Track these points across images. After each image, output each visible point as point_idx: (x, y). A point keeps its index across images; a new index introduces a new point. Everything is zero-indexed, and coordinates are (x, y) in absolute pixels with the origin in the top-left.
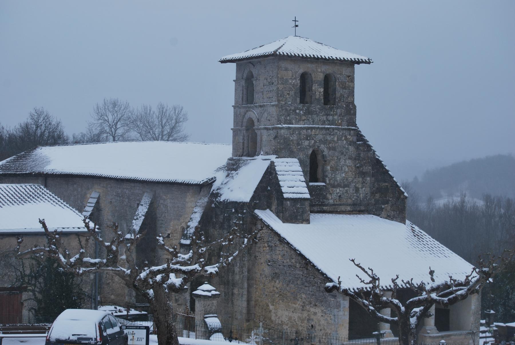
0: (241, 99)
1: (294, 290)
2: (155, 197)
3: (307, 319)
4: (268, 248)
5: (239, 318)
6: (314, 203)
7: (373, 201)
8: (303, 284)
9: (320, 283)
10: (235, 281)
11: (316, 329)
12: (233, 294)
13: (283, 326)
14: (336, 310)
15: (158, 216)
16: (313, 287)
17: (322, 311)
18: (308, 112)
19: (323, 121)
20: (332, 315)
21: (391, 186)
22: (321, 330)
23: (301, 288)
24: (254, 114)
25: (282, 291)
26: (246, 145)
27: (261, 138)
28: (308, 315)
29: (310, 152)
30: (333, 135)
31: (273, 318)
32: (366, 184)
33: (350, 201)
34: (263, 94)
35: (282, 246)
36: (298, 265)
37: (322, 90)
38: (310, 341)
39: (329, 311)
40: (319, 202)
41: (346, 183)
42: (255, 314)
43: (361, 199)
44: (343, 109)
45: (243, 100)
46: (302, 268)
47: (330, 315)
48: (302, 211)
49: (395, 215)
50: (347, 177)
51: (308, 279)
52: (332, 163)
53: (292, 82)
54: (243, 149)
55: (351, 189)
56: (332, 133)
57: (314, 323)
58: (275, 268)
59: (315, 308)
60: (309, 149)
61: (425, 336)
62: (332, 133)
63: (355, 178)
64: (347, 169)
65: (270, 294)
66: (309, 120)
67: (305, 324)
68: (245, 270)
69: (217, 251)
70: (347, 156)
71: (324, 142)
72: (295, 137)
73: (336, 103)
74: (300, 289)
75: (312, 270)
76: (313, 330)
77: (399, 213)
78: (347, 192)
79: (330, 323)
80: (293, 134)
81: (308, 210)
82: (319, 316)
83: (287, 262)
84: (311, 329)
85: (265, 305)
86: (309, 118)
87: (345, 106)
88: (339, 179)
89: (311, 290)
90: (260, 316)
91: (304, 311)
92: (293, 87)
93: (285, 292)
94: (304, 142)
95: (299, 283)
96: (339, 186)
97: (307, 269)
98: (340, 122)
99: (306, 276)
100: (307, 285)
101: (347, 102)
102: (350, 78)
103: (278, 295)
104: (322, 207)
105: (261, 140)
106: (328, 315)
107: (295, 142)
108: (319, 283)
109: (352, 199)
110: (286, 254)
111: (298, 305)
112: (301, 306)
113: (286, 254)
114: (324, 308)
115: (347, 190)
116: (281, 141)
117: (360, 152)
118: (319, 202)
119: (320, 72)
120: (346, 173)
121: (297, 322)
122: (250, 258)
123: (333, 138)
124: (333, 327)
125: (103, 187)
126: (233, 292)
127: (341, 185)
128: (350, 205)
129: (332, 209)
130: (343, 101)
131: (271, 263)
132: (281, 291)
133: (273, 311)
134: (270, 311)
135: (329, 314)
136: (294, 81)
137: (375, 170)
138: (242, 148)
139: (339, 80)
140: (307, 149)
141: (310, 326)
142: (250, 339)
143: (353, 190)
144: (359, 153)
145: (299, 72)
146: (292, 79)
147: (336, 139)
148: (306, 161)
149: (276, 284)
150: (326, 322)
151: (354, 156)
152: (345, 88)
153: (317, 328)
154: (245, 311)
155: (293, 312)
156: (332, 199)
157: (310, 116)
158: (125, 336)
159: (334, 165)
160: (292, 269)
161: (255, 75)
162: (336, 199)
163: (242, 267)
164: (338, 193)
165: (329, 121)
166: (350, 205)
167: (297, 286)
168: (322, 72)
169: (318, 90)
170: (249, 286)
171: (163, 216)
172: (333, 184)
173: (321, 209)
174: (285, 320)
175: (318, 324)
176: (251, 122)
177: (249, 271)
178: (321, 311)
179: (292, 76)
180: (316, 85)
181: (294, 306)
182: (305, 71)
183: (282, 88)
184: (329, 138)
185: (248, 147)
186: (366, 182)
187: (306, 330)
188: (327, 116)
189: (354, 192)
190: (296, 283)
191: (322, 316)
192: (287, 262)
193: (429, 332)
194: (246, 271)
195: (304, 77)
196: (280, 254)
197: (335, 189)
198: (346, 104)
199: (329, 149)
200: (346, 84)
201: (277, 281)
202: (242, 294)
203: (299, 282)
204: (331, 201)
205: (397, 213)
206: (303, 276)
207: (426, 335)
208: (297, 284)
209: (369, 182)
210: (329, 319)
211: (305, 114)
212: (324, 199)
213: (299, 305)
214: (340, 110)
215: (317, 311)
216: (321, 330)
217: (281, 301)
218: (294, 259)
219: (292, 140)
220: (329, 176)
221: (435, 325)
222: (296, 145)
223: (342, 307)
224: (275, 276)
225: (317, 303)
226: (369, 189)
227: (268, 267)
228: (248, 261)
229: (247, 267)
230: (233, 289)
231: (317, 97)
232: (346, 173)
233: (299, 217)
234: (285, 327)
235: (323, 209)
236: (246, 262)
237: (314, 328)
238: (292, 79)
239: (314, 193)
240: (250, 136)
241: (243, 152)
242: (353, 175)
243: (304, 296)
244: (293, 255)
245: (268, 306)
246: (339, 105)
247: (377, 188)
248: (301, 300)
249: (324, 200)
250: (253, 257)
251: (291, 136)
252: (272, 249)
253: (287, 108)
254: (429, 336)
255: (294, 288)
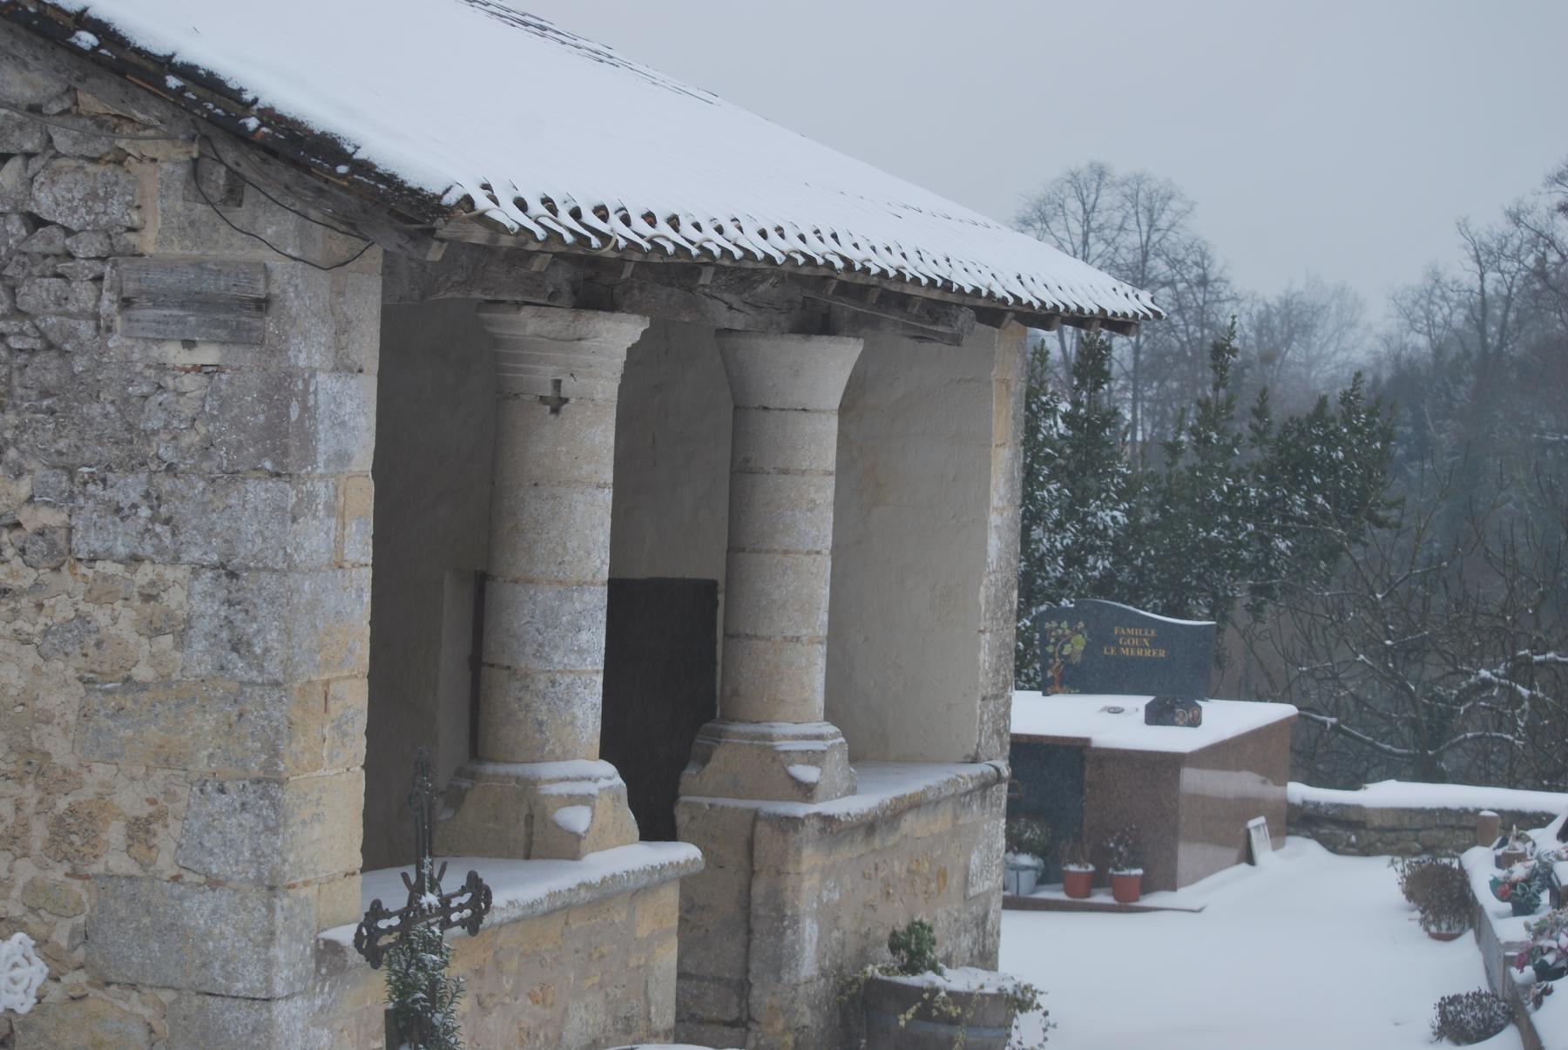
14: (258, 492)
47: (145, 573)
61: (794, 822)
79: (143, 673)
158: (1502, 817)
193: (808, 773)
207: (801, 810)
223: (321, 459)
254: (818, 815)
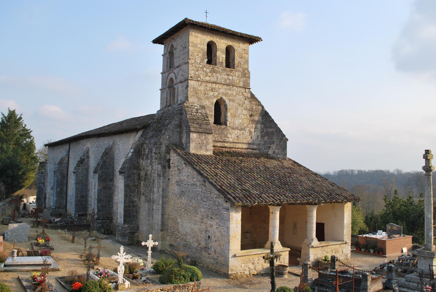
0: (166, 67)
1: (195, 205)
2: (114, 144)
3: (204, 230)
4: (177, 171)
5: (156, 228)
6: (217, 140)
7: (263, 142)
8: (202, 199)
9: (216, 198)
10: (154, 199)
11: (212, 240)
12: (153, 209)
13: (187, 236)
15: (115, 156)
16: (210, 202)
17: (217, 223)
18: (213, 71)
19: (225, 79)
20: (225, 228)
21: (276, 131)
22: (216, 241)
23: (201, 203)
24: (172, 75)
25: (187, 206)
26: (168, 99)
27: (178, 90)
28: (206, 227)
29: (215, 101)
30: (233, 90)
31: (180, 229)
32: (258, 129)
33: (245, 141)
34: (179, 58)
35: (187, 168)
36: (198, 184)
37: (224, 56)
38: (207, 250)
39: (222, 223)
40: (221, 140)
41: (243, 127)
42: (168, 226)
43: (254, 140)
44: (240, 72)
45: (167, 67)
46: (202, 185)
48: (206, 143)
49: (279, 152)
50: (243, 122)
51: (206, 195)
52: (232, 111)
53: (201, 46)
54: (167, 102)
55: (246, 132)
56: (232, 89)
57: (211, 234)
58: (182, 187)
59: (211, 221)
60: (214, 98)
62: (232, 89)
63: (250, 124)
64: (243, 117)
65: (179, 209)
66: (213, 77)
67: (203, 235)
68: (161, 189)
69: (144, 177)
70: (243, 107)
71: (226, 95)
72: (202, 88)
73: (235, 68)
74: (200, 204)
75: (209, 187)
76: (209, 241)
77: (282, 151)
78: (243, 134)
79: (224, 234)
80: (201, 85)
81: (211, 142)
82: (215, 228)
83: (190, 181)
84: (208, 239)
85: (175, 218)
86: (214, 75)
87: (241, 70)
88: (237, 123)
89: (208, 204)
90: (171, 227)
91: (203, 223)
92: (201, 50)
93: (189, 207)
94: (210, 93)
95: (199, 199)
96: (237, 128)
97: (205, 186)
98: (238, 81)
99: (204, 192)
100: (205, 200)
101: (243, 68)
102: (245, 51)
103: (183, 210)
104: (224, 143)
105: (178, 92)
106: (222, 227)
107: (202, 91)
108: (214, 198)
109: (247, 140)
110: (189, 174)
111: (198, 218)
112: (200, 219)
113: (189, 174)
114: (218, 221)
115: (243, 132)
116: (191, 90)
117: (253, 105)
118: (221, 140)
119: (223, 43)
120: (243, 119)
121: (197, 233)
122: (164, 180)
123: (232, 93)
124: (226, 238)
125: (91, 143)
126: (153, 208)
127: (239, 128)
128: (245, 143)
129: (232, 146)
130: (241, 67)
131: (179, 183)
132: (186, 207)
133: (180, 223)
134: (178, 223)
135: (223, 226)
136: (202, 46)
137: (264, 120)
138: (166, 101)
139: (237, 51)
140: (212, 98)
141: (207, 237)
142: (118, 255)
143: (248, 133)
144: (252, 106)
145: (206, 40)
146: (200, 44)
147: (234, 93)
148: (211, 107)
149: (183, 200)
150: (220, 234)
151: (248, 108)
152: (242, 58)
153: (213, 239)
154: (160, 223)
155: (194, 224)
156: (231, 138)
157: (215, 74)
159: (234, 113)
160: (194, 187)
161: (175, 47)
162: (235, 138)
163: (159, 188)
164: (236, 134)
165: (230, 79)
166: (245, 143)
167: (197, 202)
168: (224, 43)
169: (221, 56)
170: (163, 203)
171: (118, 156)
172: (233, 127)
173: (223, 145)
174: (189, 231)
175: (213, 236)
176: (172, 80)
177: (163, 190)
178: (216, 223)
179: (201, 42)
180: (220, 52)
181: (195, 218)
182: (211, 40)
183: (193, 50)
184: (230, 92)
185: (170, 100)
186: (258, 128)
187: (204, 240)
188: (228, 76)
189: (249, 134)
190: (197, 199)
191: (217, 228)
192: (191, 181)
194: (161, 190)
195: (211, 47)
196: (185, 175)
197: (234, 131)
198: (243, 69)
199: (230, 100)
200: (242, 55)
201: (184, 198)
202: (158, 209)
203: (199, 198)
204: (231, 140)
205: (280, 151)
206: (202, 192)
208: (198, 200)
209: (260, 128)
210: (222, 230)
211: (211, 72)
212: (226, 137)
213: (199, 218)
214: (238, 73)
215: (213, 223)
216: (216, 241)
217: (185, 215)
218: (195, 178)
219: (200, 90)
220: (229, 121)
221: (316, 237)
222: (203, 94)
223: (234, 220)
224: (182, 193)
225: (213, 216)
226: (260, 133)
227: (177, 187)
228: (163, 182)
229: (161, 188)
230: (153, 206)
231: (221, 61)
232: (243, 119)
233: (203, 147)
234: (188, 237)
235: (224, 145)
236: (161, 184)
237: (210, 239)
238: (200, 44)
239: (217, 132)
240: (172, 92)
241: (166, 104)
242: (248, 121)
243: (202, 210)
244: (195, 175)
245: (177, 219)
246: (237, 69)
247: (266, 132)
248: (201, 214)
249: (226, 138)
250: (167, 179)
251: (199, 87)
252: (180, 172)
253: (196, 65)
255: (195, 204)
